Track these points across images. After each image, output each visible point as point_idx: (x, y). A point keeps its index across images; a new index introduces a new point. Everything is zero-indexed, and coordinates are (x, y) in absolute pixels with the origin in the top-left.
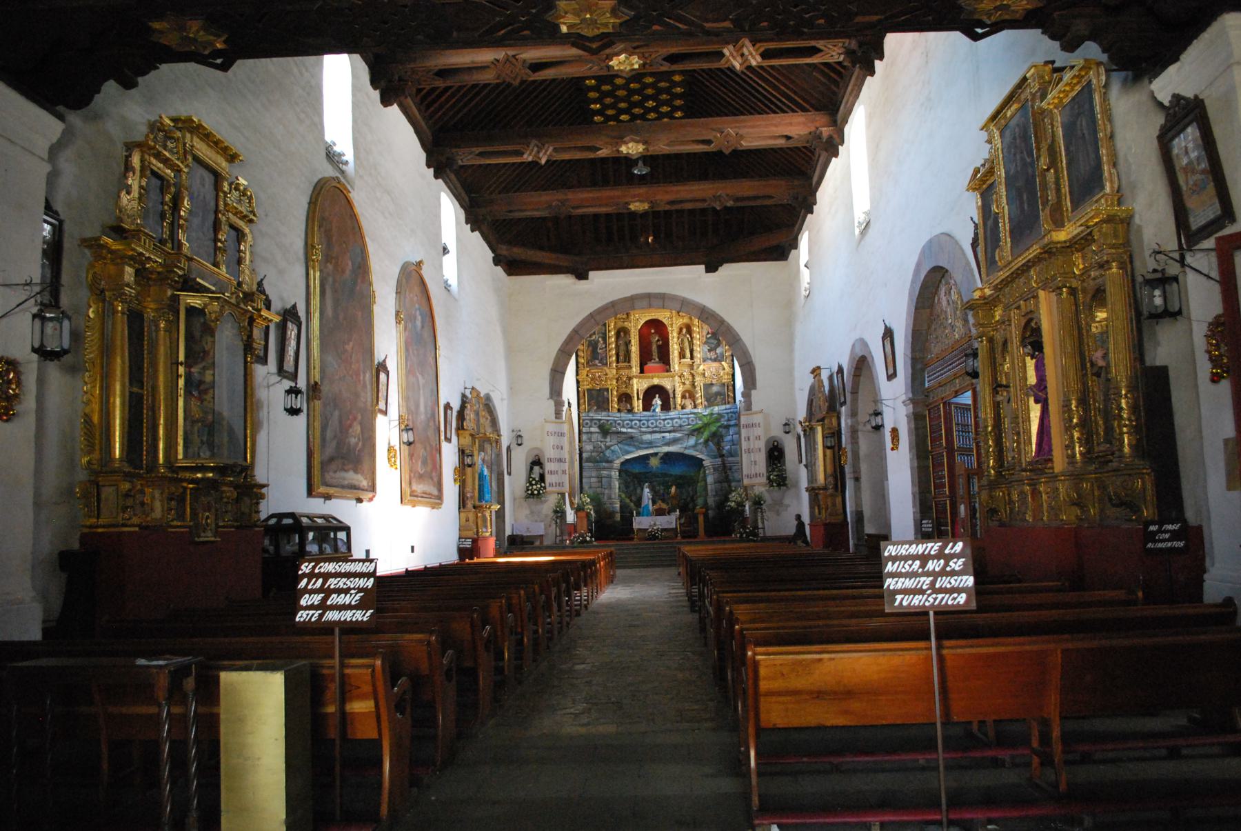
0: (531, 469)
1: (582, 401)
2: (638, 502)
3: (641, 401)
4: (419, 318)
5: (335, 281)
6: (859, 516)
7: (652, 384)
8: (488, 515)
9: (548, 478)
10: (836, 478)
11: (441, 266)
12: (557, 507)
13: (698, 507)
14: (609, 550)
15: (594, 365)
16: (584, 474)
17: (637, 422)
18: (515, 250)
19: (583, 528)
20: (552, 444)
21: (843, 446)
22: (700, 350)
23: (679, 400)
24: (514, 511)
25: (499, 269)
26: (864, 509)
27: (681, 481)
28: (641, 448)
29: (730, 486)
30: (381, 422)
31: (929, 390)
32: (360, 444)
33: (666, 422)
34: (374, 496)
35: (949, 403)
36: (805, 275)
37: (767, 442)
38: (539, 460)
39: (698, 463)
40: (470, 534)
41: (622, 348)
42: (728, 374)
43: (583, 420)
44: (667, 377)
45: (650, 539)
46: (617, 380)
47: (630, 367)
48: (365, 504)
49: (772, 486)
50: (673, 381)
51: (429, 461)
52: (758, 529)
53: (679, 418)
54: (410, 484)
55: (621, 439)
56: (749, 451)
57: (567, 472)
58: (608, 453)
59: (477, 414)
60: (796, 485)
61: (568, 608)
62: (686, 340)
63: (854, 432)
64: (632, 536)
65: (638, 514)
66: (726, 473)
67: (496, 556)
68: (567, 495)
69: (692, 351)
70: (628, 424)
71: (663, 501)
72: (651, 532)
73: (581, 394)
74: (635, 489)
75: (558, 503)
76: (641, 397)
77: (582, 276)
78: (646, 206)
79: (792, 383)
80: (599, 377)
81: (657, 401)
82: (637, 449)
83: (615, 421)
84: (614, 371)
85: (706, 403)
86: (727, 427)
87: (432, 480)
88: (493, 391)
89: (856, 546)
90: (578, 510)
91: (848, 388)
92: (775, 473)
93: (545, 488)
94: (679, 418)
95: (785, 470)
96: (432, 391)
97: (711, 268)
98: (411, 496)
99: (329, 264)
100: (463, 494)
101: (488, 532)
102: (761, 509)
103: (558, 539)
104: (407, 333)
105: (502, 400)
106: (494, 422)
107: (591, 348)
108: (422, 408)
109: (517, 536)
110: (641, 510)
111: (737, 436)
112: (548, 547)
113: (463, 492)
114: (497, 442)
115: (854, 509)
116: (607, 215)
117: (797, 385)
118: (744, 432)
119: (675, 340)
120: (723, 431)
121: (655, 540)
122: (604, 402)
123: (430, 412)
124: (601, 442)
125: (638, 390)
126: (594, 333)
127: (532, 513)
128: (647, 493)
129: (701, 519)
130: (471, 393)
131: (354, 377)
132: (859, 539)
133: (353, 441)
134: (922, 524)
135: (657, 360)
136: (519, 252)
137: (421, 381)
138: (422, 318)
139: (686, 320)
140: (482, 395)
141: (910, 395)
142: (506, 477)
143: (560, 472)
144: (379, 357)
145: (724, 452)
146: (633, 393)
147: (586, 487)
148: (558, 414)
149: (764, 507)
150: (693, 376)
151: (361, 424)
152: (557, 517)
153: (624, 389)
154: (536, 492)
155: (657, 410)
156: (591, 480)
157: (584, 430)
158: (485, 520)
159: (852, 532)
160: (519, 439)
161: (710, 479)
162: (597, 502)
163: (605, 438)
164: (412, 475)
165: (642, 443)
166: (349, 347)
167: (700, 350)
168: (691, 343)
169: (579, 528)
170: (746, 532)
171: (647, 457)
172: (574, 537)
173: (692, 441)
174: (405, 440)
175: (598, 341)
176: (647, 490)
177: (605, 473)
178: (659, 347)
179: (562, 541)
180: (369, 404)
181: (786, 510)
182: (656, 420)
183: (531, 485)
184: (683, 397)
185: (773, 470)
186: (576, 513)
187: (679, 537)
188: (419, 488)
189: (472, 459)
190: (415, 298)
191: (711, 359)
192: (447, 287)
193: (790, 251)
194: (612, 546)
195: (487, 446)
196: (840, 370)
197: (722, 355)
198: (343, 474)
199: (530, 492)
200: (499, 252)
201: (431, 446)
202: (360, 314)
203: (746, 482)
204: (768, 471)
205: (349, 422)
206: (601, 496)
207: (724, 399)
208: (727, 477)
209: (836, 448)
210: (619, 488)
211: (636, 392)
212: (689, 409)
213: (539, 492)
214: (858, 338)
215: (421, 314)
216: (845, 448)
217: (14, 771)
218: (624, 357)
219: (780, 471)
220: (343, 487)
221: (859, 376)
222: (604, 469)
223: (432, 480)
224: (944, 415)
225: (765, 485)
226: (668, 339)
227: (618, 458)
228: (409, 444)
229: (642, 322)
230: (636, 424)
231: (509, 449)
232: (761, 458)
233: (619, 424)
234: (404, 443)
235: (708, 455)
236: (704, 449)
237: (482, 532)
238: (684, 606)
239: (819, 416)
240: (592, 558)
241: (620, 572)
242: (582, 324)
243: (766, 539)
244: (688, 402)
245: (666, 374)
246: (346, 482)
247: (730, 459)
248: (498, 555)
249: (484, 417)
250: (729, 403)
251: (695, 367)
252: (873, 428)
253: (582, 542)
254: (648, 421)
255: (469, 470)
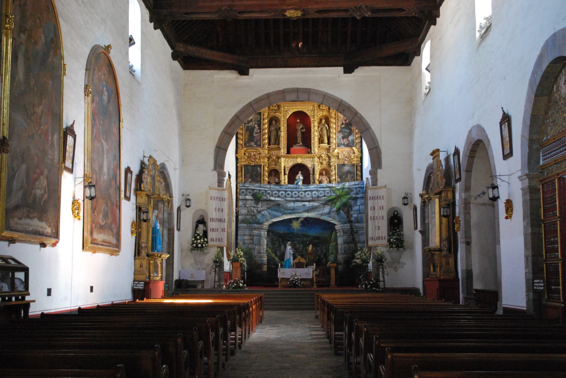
0: (197, 227)
1: (239, 174)
2: (282, 257)
3: (287, 176)
4: (106, 93)
5: (27, 51)
6: (469, 274)
7: (296, 163)
8: (159, 262)
9: (211, 235)
10: (450, 244)
11: (127, 53)
12: (216, 258)
13: (329, 262)
14: (260, 295)
15: (250, 146)
16: (240, 232)
17: (283, 192)
18: (190, 48)
19: (237, 276)
20: (214, 208)
21: (457, 215)
22: (335, 137)
23: (317, 176)
24: (181, 259)
25: (176, 63)
26: (473, 268)
27: (316, 241)
28: (285, 214)
29: (356, 246)
30: (67, 180)
31: (543, 168)
32: (46, 196)
33: (306, 193)
34: (57, 242)
35: (563, 178)
36: (427, 77)
37: (389, 212)
38: (203, 219)
39: (330, 227)
40: (143, 277)
41: (274, 133)
42: (357, 157)
43: (240, 189)
44: (308, 158)
45: (291, 287)
46: (269, 158)
47: (279, 149)
48: (48, 248)
49: (392, 247)
50: (313, 161)
51: (110, 215)
52: (380, 281)
53: (317, 191)
54: (92, 233)
55: (270, 206)
56: (374, 218)
57: (226, 230)
58: (259, 216)
59: (153, 178)
60: (412, 247)
61: (224, 347)
62: (324, 129)
63: (467, 204)
64: (276, 283)
65: (282, 266)
66: (353, 235)
67: (163, 298)
68: (225, 248)
69: (329, 138)
70: (276, 194)
71: (302, 256)
72: (293, 281)
73: (239, 169)
74: (280, 246)
75: (218, 254)
76: (287, 173)
77: (244, 72)
78: (299, 14)
79: (411, 165)
80: (254, 155)
81: (300, 177)
82: (283, 214)
83: (266, 191)
84: (267, 151)
85: (339, 179)
86: (356, 199)
87: (112, 231)
88: (168, 161)
89: (466, 299)
90: (234, 261)
91: (463, 167)
92: (394, 237)
93: (207, 242)
94: (317, 191)
95: (403, 235)
96: (115, 156)
97: (348, 70)
98: (91, 243)
99: (22, 35)
100: (139, 244)
101: (159, 278)
102: (382, 265)
103: (217, 284)
104: (94, 105)
105: (175, 169)
106: (168, 187)
107: (248, 132)
108: (105, 170)
109: (183, 280)
110: (283, 263)
111: (364, 206)
112: (209, 291)
113: (139, 243)
114: (169, 202)
115: (465, 268)
116: (266, 21)
117: (415, 167)
118: (370, 203)
119: (316, 128)
120: (352, 202)
121: (295, 287)
122: (257, 176)
123: (112, 174)
124: (254, 207)
125: (284, 167)
126: (251, 120)
127: (196, 262)
128: (289, 249)
129: (333, 272)
130: (148, 161)
131: (43, 136)
132: (468, 293)
133: (39, 192)
134: (533, 283)
135: (301, 143)
136: (192, 50)
137: (106, 147)
138: (108, 93)
139: (325, 113)
140: (158, 163)
141: (527, 172)
142: (176, 232)
143: (220, 230)
144: (67, 122)
145: (352, 219)
146: (281, 169)
147: (240, 243)
148: (220, 183)
149: (385, 264)
150: (329, 158)
151: (47, 178)
152: (216, 267)
153: (273, 166)
154: (200, 245)
155: (299, 184)
156: (244, 237)
157: (241, 197)
158: (156, 266)
159: (462, 286)
160: (187, 202)
161: (340, 240)
162: (248, 255)
163: (258, 204)
164: (94, 225)
165: (286, 209)
166: (39, 110)
167: (335, 137)
168: (329, 131)
169: (233, 276)
170: (369, 284)
171: (290, 220)
172: (230, 283)
173: (327, 209)
174: (88, 195)
175: (254, 127)
176: (289, 247)
177: (256, 232)
178: (303, 133)
179: (220, 286)
180: (56, 161)
181: (402, 267)
182: (299, 192)
183: (196, 239)
184: (321, 174)
185: (393, 234)
186: (232, 263)
187: (315, 287)
188: (99, 237)
189: (147, 216)
190: (103, 77)
191: (344, 145)
192: (132, 71)
193: (413, 58)
194: (262, 292)
195: (161, 205)
196: (457, 152)
197: (353, 141)
198: (28, 221)
199: (195, 245)
200: (177, 48)
201: (112, 203)
202: (51, 82)
203: (370, 243)
204: (389, 235)
205: (36, 175)
206: (253, 251)
207: (353, 177)
208: (354, 239)
209: (451, 217)
210: (267, 244)
211: (283, 168)
212: (325, 184)
213: (202, 245)
214: (475, 124)
215: (107, 90)
216: (459, 217)
217: (224, 286)
218: (274, 140)
219: (398, 235)
220: (27, 232)
221: (474, 157)
222: (255, 229)
223: (112, 231)
224: (559, 189)
225: (386, 246)
226: (310, 127)
227: (267, 221)
228: (91, 198)
229: (290, 113)
230: (282, 194)
231: (179, 209)
232: (384, 225)
233: (269, 194)
234: (87, 197)
235: (339, 221)
236: (337, 216)
237: (154, 276)
238: (326, 349)
239: (437, 190)
240: (245, 301)
241: (266, 313)
242: (243, 111)
243: (385, 290)
244: (324, 178)
245: (308, 155)
246: (31, 229)
247: (356, 225)
248: (166, 296)
249: (159, 181)
250: (357, 180)
251: (331, 151)
252: (490, 199)
253: (236, 287)
254: (292, 192)
255: (144, 224)
